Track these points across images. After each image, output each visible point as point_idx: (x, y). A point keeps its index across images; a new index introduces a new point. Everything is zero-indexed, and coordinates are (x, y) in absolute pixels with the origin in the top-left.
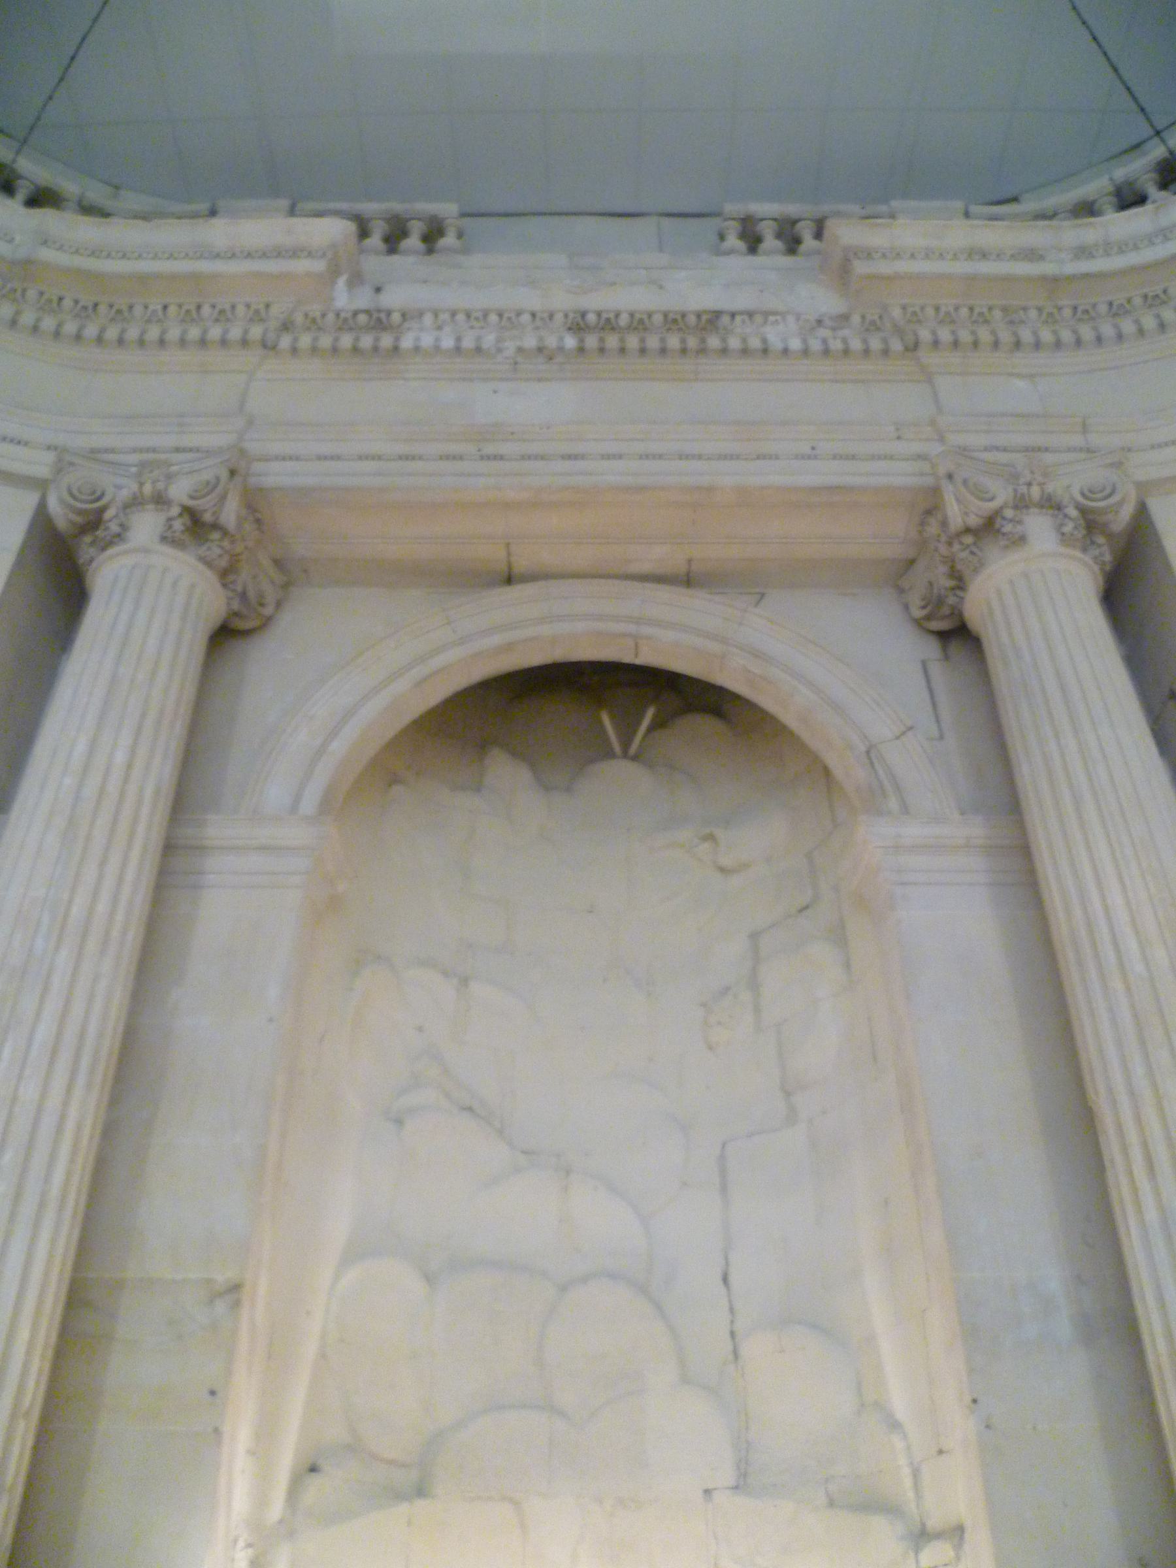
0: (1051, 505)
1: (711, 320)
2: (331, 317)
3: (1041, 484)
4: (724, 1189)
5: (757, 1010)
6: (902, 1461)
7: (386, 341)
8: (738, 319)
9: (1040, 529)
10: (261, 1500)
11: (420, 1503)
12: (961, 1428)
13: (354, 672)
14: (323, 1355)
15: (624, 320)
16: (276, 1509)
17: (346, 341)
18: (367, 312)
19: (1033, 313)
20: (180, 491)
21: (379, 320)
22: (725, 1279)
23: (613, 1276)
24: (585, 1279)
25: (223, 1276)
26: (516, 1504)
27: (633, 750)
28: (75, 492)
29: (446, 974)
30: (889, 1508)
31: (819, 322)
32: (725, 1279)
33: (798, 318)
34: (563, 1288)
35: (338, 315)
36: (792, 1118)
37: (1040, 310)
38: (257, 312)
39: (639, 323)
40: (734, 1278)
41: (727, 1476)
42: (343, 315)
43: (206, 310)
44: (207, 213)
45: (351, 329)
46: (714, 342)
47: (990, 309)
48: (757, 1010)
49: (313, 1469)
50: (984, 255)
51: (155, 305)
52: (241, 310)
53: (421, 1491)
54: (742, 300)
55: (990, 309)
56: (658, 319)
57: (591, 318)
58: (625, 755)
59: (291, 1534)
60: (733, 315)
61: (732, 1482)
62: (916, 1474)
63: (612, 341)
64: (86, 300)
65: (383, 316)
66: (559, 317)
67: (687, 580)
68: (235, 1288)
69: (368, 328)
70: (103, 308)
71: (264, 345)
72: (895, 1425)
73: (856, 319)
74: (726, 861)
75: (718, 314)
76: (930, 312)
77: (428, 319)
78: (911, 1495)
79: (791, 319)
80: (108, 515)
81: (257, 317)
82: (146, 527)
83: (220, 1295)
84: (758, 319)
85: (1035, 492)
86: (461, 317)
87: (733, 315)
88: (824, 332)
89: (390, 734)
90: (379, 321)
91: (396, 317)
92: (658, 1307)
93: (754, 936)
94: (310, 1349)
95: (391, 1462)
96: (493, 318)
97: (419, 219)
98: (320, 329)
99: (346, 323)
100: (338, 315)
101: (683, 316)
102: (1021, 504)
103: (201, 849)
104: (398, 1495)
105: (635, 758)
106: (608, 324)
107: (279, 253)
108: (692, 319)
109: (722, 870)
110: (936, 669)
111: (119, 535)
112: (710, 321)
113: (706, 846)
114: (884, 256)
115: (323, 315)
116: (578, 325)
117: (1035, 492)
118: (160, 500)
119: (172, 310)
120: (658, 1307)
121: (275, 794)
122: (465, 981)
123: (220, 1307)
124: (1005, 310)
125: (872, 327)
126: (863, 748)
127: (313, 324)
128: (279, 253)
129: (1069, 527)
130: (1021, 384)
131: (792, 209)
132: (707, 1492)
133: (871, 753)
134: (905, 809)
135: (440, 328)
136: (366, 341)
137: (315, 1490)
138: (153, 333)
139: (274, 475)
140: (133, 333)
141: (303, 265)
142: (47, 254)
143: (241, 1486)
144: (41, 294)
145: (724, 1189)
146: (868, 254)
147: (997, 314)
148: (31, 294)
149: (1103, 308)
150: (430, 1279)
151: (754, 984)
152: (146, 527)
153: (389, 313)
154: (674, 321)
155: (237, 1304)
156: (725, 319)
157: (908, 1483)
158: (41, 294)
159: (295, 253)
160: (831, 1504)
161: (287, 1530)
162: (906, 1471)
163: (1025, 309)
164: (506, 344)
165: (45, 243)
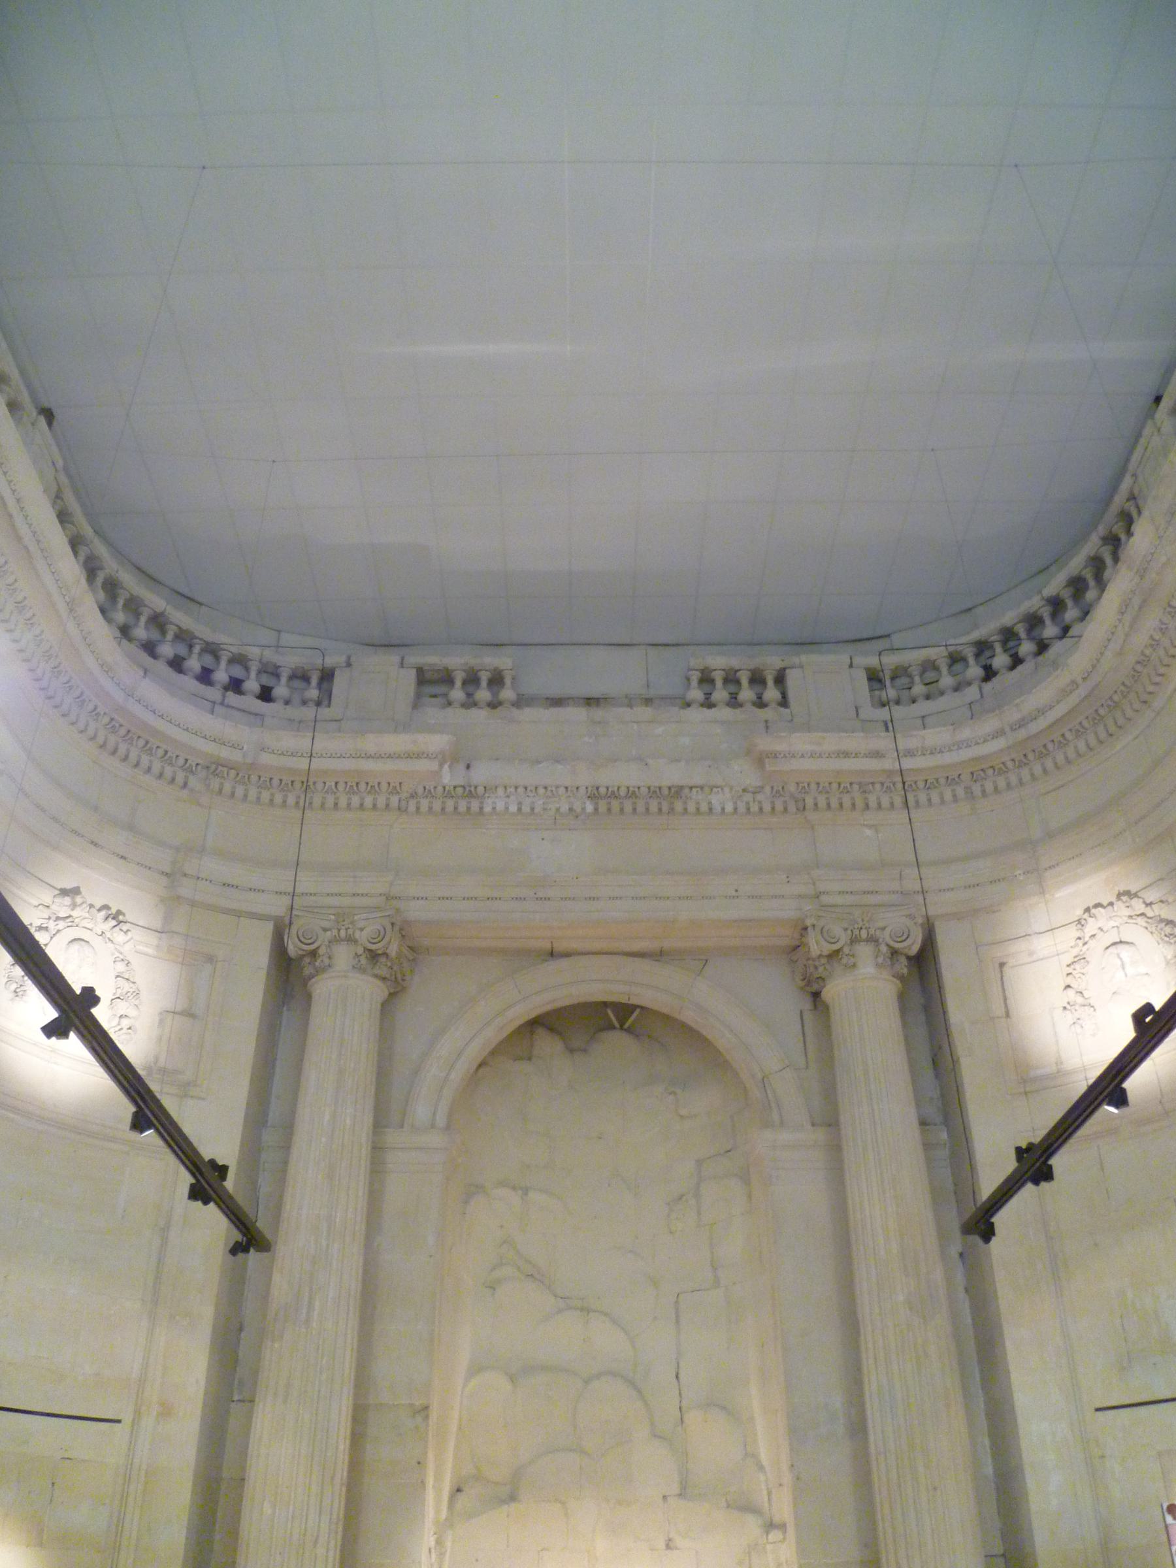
0: (873, 940)
1: (677, 792)
2: (440, 789)
3: (868, 929)
4: (677, 1321)
5: (699, 1213)
6: (763, 1487)
7: (475, 805)
8: (694, 790)
9: (864, 952)
10: (438, 1511)
11: (514, 1505)
12: (787, 1478)
13: (462, 1020)
14: (460, 1428)
15: (623, 792)
16: (444, 1513)
17: (450, 804)
18: (464, 787)
19: (878, 786)
20: (363, 937)
22: (677, 1377)
23: (613, 1374)
24: (598, 1376)
25: (418, 1403)
26: (563, 1503)
27: (626, 1026)
29: (514, 1188)
30: (754, 1510)
31: (744, 790)
32: (677, 1377)
33: (731, 788)
34: (587, 1382)
36: (717, 1283)
37: (882, 784)
38: (395, 788)
39: (632, 794)
40: (681, 1376)
41: (675, 1488)
43: (362, 786)
46: (679, 805)
47: (851, 784)
48: (699, 1213)
49: (459, 1490)
50: (846, 754)
52: (384, 786)
53: (512, 1498)
54: (698, 780)
55: (851, 784)
56: (644, 790)
57: (603, 791)
58: (621, 1028)
59: (452, 1526)
60: (691, 788)
61: (677, 1491)
62: (769, 1494)
63: (615, 804)
66: (582, 791)
67: (658, 955)
68: (426, 1408)
72: (761, 1468)
73: (768, 789)
74: (683, 1112)
75: (681, 788)
76: (813, 786)
77: (500, 791)
78: (766, 1505)
79: (727, 790)
80: (321, 952)
81: (395, 791)
82: (343, 956)
83: (419, 1412)
84: (707, 790)
85: (864, 934)
86: (521, 790)
87: (691, 788)
88: (748, 797)
90: (470, 792)
91: (481, 790)
92: (639, 1392)
93: (699, 1163)
94: (454, 1428)
95: (497, 1483)
96: (541, 791)
101: (660, 788)
102: (854, 941)
104: (503, 1502)
105: (629, 1031)
106: (613, 795)
107: (409, 756)
108: (666, 792)
109: (682, 1116)
110: (808, 1017)
111: (329, 966)
112: (677, 792)
113: (671, 1097)
114: (785, 756)
116: (594, 795)
117: (864, 934)
118: (350, 940)
119: (341, 787)
120: (639, 1392)
121: (421, 1111)
122: (526, 1191)
123: (419, 1419)
124: (860, 784)
125: (777, 794)
126: (759, 1076)
127: (428, 794)
128: (409, 756)
129: (880, 960)
130: (868, 832)
131: (734, 662)
132: (665, 1497)
133: (764, 1082)
134: (782, 1124)
135: (508, 797)
137: (462, 1501)
139: (415, 911)
141: (424, 765)
142: (266, 759)
143: (433, 1504)
145: (677, 1321)
146: (775, 756)
147: (856, 787)
148: (254, 778)
149: (921, 784)
150: (512, 1379)
151: (697, 1196)
152: (343, 956)
154: (655, 792)
155: (427, 1417)
156: (686, 791)
157: (766, 1499)
159: (419, 756)
160: (728, 1506)
161: (449, 1523)
162: (765, 1492)
163: (873, 783)
164: (550, 806)
165: (263, 749)
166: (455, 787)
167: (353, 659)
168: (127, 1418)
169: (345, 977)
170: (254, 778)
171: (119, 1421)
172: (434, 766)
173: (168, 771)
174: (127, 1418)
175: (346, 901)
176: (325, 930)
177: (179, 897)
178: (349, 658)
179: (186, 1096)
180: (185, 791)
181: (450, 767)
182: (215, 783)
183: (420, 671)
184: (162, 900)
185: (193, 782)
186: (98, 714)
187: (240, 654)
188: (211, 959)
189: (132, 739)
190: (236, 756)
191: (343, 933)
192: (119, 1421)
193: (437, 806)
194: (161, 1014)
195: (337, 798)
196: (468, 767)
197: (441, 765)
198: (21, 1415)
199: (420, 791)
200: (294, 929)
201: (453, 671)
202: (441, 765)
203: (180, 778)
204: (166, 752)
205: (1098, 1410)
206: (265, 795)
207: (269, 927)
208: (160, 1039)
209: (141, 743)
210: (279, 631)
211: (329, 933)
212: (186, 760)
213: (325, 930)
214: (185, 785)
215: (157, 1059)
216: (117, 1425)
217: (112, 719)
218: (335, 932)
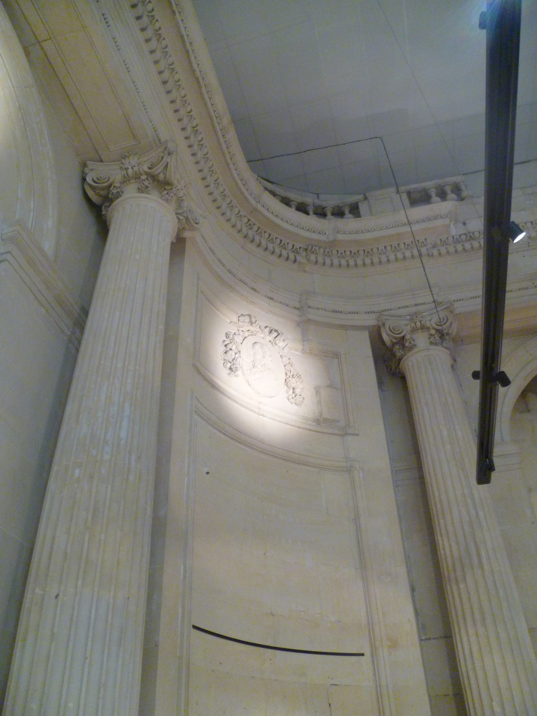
2: (451, 239)
17: (459, 247)
18: (465, 234)
21: (470, 236)
28: (392, 329)
35: (453, 237)
42: (455, 237)
43: (402, 246)
44: (363, 199)
45: (460, 242)
51: (381, 247)
64: (354, 250)
65: (471, 234)
69: (466, 241)
70: (361, 252)
71: (428, 255)
82: (421, 340)
89: (517, 398)
97: (449, 185)
98: (447, 244)
99: (457, 241)
100: (453, 237)
103: (330, 386)
107: (429, 219)
115: (447, 239)
118: (423, 328)
119: (389, 248)
127: (444, 243)
128: (429, 219)
136: (468, 246)
138: (384, 258)
140: (376, 260)
141: (440, 222)
142: (340, 237)
144: (338, 251)
152: (421, 340)
153: (473, 233)
158: (338, 251)
159: (436, 218)
166: (460, 236)
167: (367, 194)
168: (367, 651)
169: (428, 349)
170: (335, 252)
171: (362, 655)
172: (447, 221)
173: (284, 253)
174: (367, 651)
175: (413, 310)
176: (406, 325)
177: (309, 320)
178: (365, 195)
179: (346, 434)
180: (296, 264)
181: (454, 224)
182: (313, 257)
183: (409, 193)
184: (298, 324)
185: (299, 258)
186: (241, 216)
187: (302, 203)
188: (336, 355)
189: (261, 233)
190: (323, 238)
191: (418, 324)
192: (362, 655)
193: (451, 249)
194: (315, 388)
195: (387, 256)
196: (464, 224)
197: (451, 221)
198: (270, 650)
199: (439, 242)
200: (387, 326)
201: (429, 189)
202: (451, 221)
203: (292, 256)
204: (281, 241)
205: (195, 627)
206: (343, 262)
207: (365, 336)
208: (319, 402)
209: (267, 235)
210: (318, 194)
211: (409, 327)
212: (293, 246)
213: (406, 325)
214: (295, 261)
215: (321, 414)
216: (361, 657)
217: (249, 220)
218: (413, 325)
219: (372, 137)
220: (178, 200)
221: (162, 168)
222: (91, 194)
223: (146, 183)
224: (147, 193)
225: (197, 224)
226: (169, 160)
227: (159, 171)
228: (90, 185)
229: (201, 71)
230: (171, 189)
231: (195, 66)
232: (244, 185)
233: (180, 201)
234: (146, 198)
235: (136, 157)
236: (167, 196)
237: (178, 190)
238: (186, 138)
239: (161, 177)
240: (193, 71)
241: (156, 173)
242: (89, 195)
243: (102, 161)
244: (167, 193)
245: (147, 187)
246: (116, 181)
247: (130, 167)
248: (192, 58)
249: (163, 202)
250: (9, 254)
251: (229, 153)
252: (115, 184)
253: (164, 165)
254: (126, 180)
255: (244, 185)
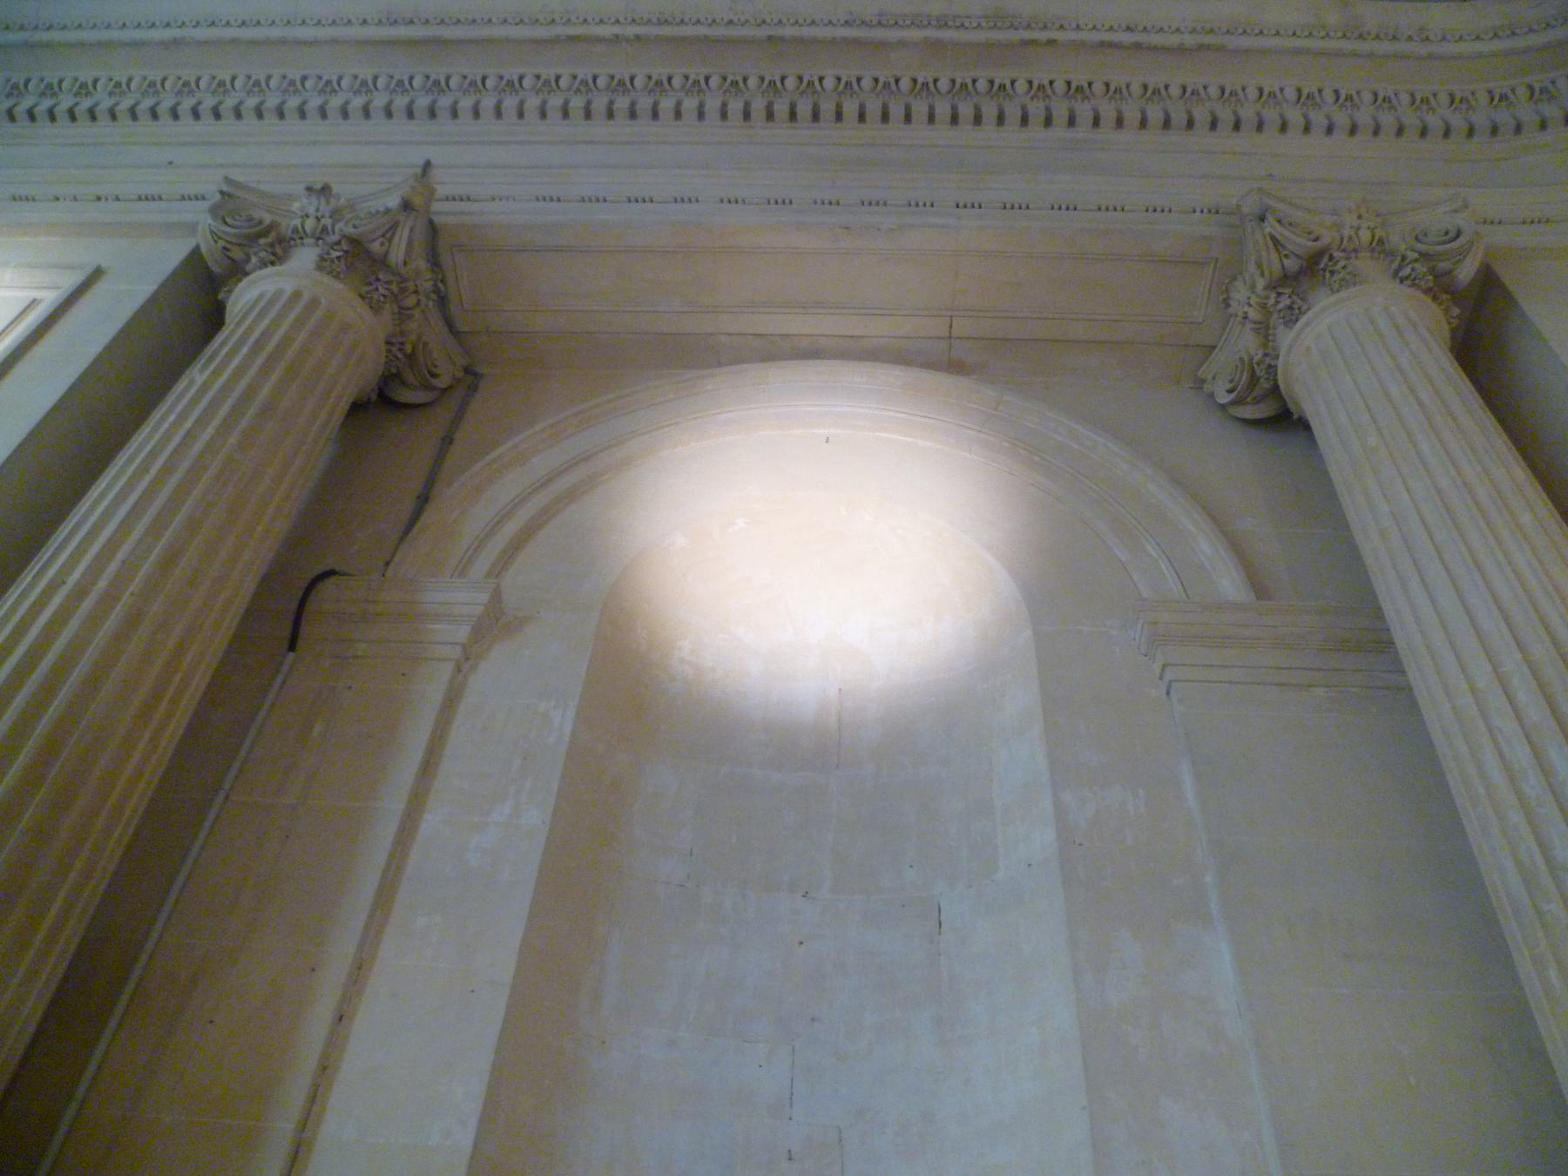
219: (287, 633)
220: (1373, 251)
221: (1274, 256)
222: (1249, 412)
223: (1285, 301)
224: (1302, 313)
225: (1458, 234)
226: (1268, 230)
227: (1277, 261)
228: (1232, 403)
229: (1194, 31)
230: (1331, 258)
231: (1174, 40)
232: (1514, 34)
233: (1379, 247)
234: (1307, 324)
235: (1239, 284)
236: (1336, 277)
237: (1350, 238)
238: (1307, 129)
239: (1292, 264)
240: (1181, 50)
241: (1277, 268)
242: (1247, 416)
243: (1214, 348)
244: (1332, 273)
245: (1290, 308)
246: (1252, 352)
247: (1246, 308)
248: (1156, 39)
249: (1343, 294)
250: (1168, 669)
251: (1410, 38)
252: (1256, 359)
253: (1270, 243)
254: (1264, 331)
255: (1514, 34)
